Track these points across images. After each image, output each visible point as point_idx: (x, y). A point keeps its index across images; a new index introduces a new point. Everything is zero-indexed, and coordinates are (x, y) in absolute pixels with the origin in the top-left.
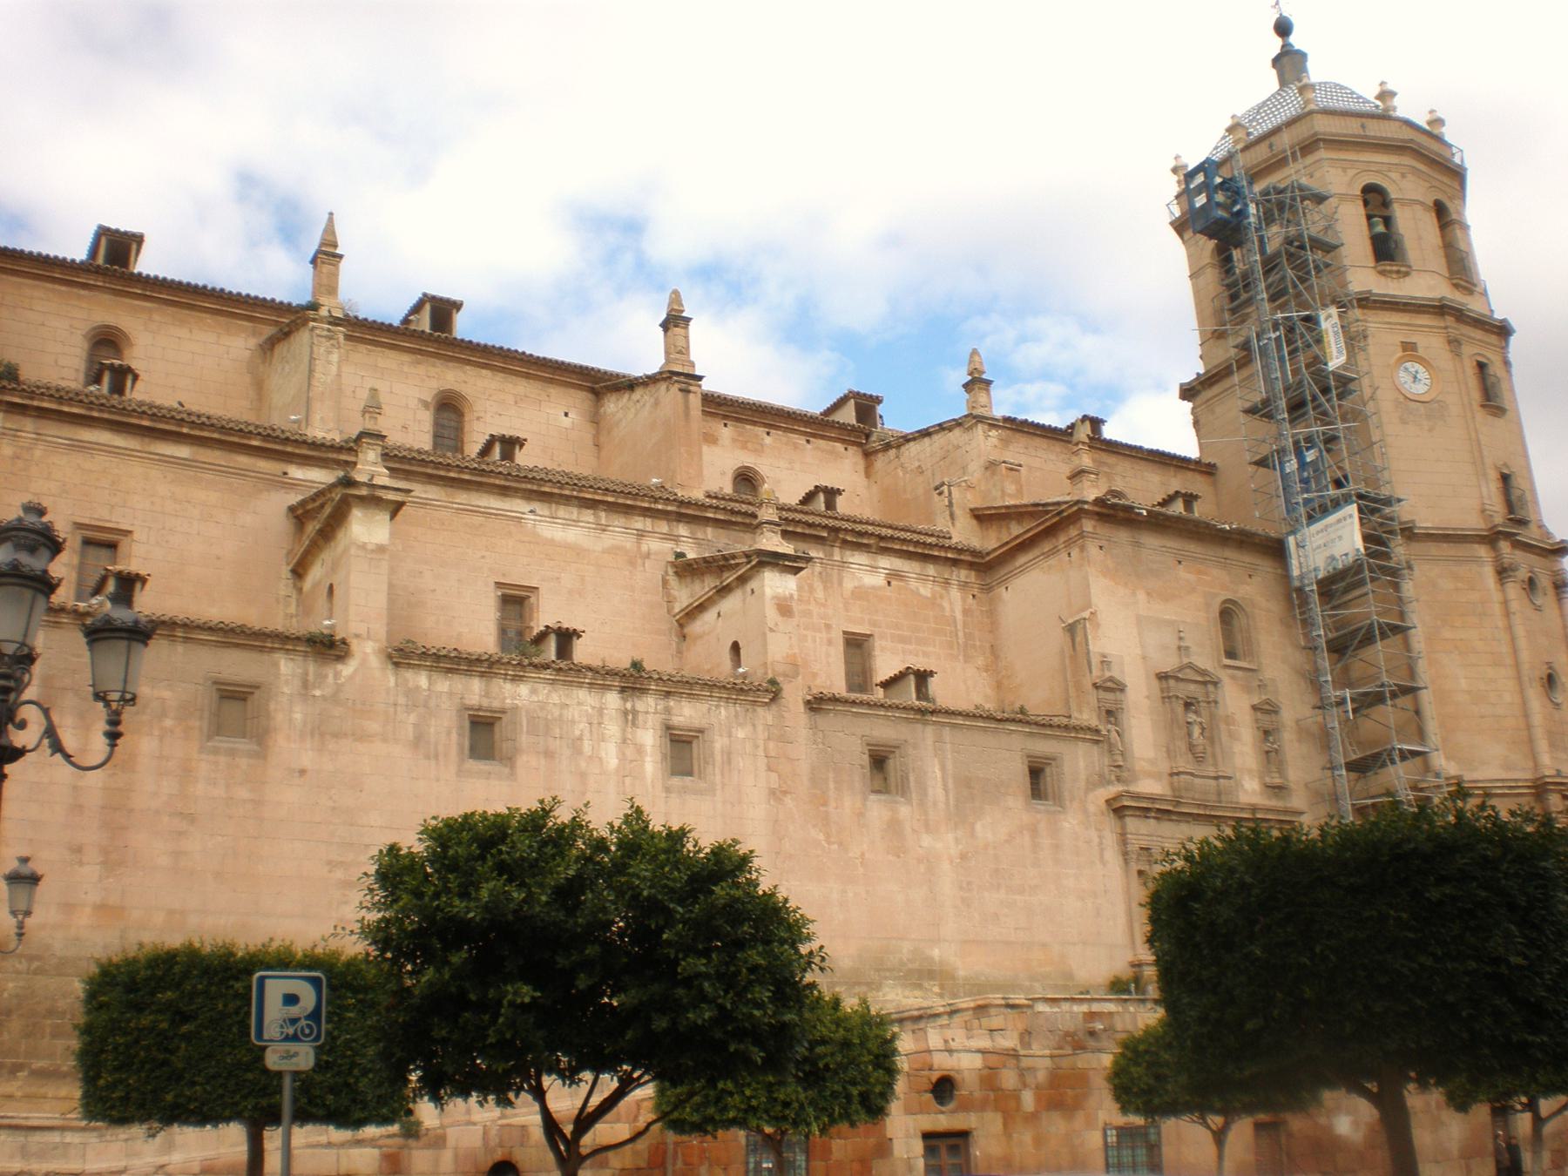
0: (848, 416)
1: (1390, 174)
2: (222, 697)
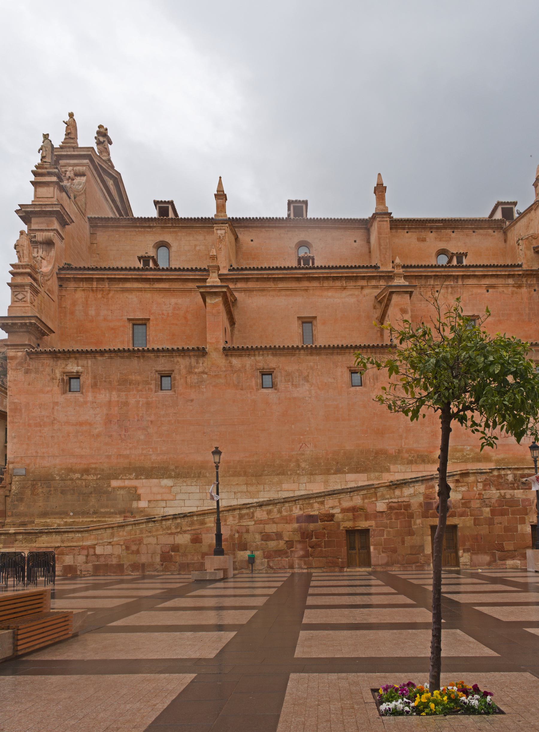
2: (352, 373)
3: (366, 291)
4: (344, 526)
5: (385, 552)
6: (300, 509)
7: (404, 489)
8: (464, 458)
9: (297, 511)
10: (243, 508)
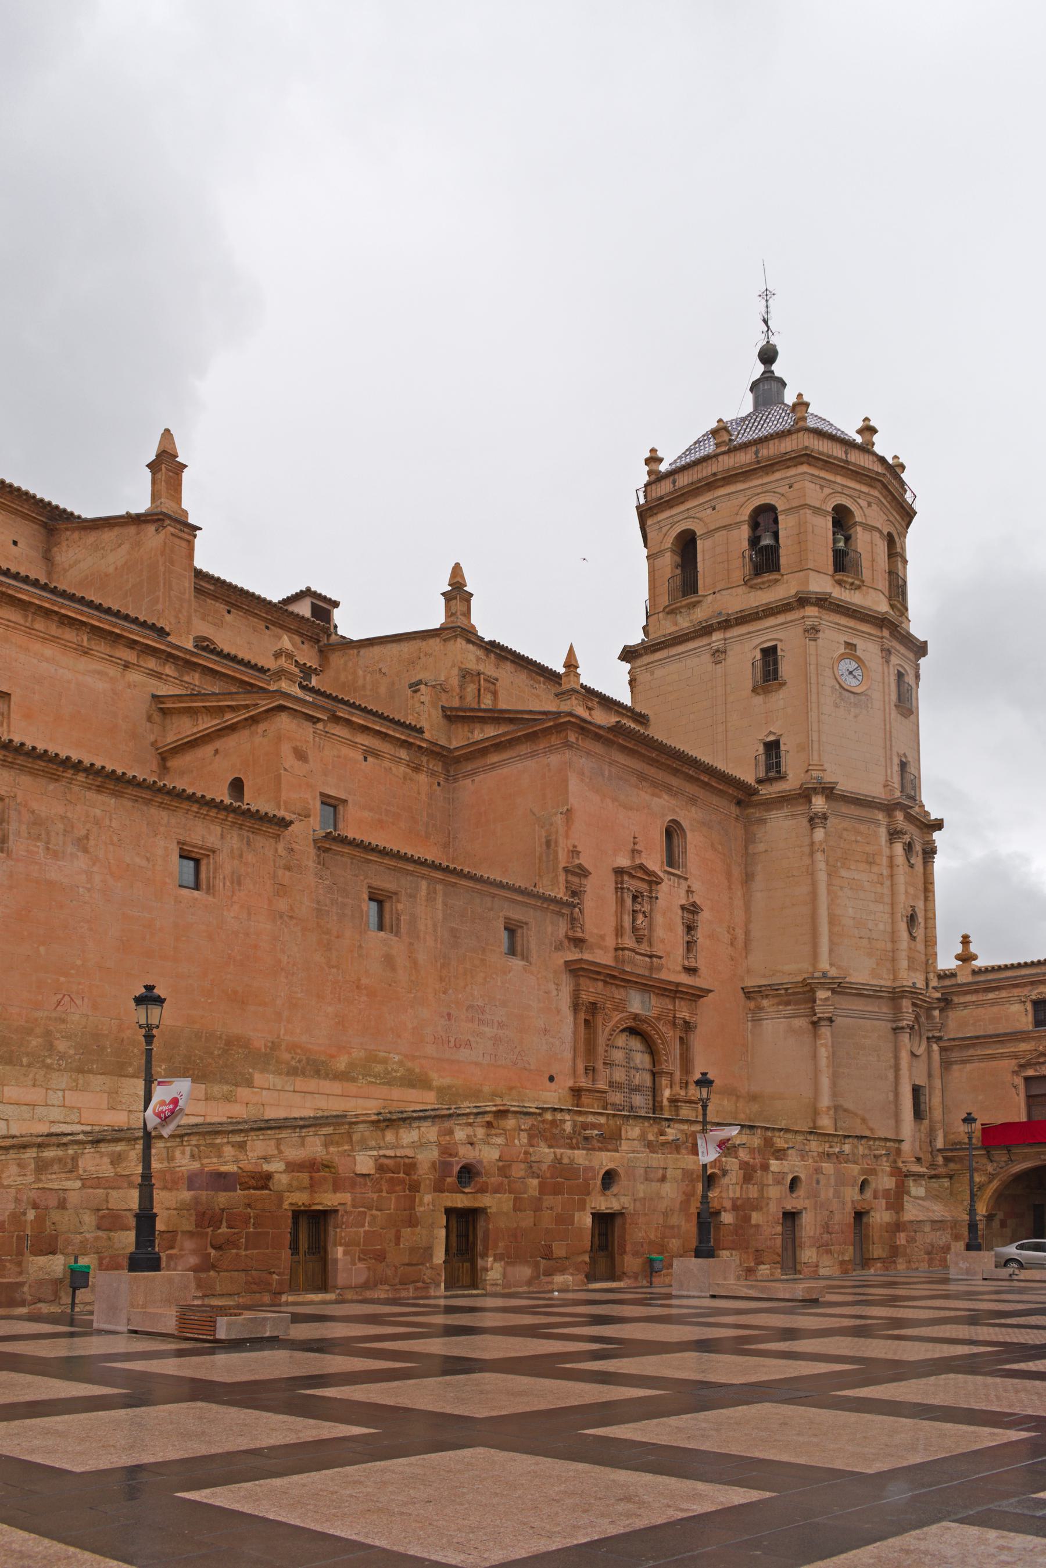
0: (304, 609)
1: (858, 500)
3: (133, 676)
4: (290, 1201)
5: (364, 1260)
6: (192, 1156)
7: (401, 1131)
8: (388, 1076)
9: (184, 1162)
10: (48, 1145)
